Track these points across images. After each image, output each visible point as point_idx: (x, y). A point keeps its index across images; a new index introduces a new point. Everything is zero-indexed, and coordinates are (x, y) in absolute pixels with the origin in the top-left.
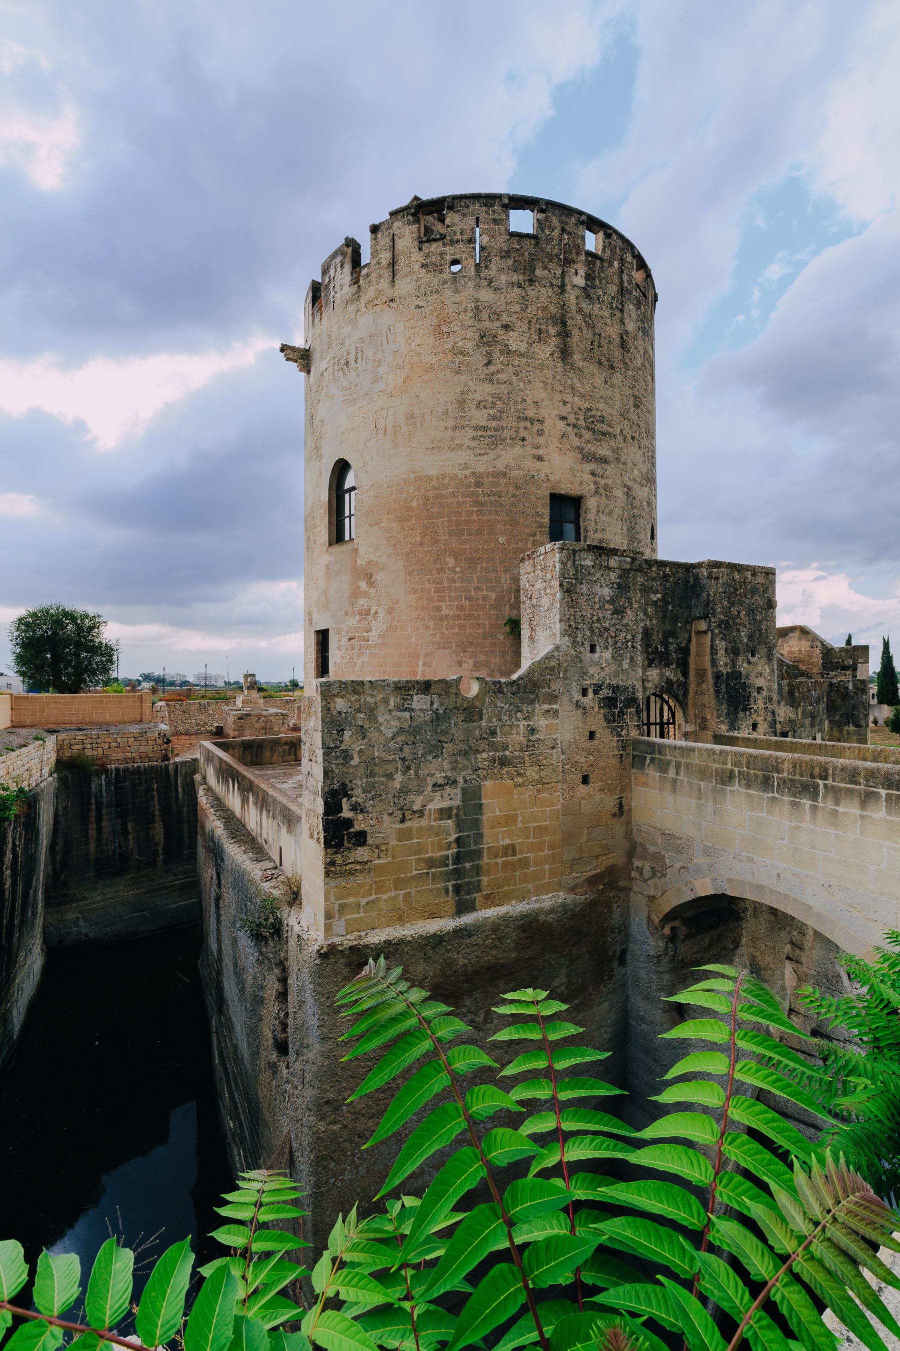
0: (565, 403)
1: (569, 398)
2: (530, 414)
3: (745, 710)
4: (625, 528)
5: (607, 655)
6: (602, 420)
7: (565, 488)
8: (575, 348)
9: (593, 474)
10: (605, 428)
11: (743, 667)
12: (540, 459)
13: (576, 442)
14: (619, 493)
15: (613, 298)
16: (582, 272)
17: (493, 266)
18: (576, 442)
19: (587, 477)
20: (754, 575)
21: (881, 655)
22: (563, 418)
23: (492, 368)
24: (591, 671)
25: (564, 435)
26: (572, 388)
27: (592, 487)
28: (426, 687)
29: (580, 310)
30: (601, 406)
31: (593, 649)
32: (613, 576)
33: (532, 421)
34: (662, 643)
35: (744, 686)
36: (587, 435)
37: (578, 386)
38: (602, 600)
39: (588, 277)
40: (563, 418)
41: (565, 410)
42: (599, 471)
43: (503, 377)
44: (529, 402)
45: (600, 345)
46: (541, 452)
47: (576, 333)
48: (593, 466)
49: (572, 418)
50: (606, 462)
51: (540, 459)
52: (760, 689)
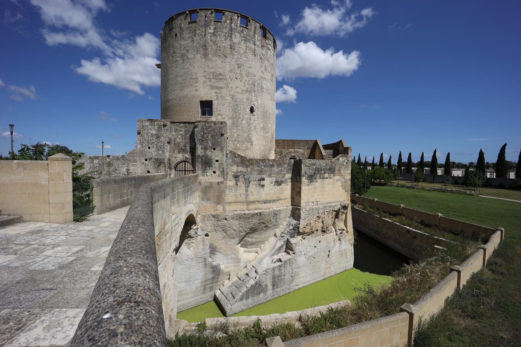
0: (205, 71)
1: (207, 70)
2: (194, 77)
3: (210, 167)
4: (231, 109)
5: (154, 149)
6: (220, 74)
7: (204, 99)
8: (209, 53)
9: (216, 93)
10: (221, 77)
11: (209, 153)
12: (197, 90)
13: (209, 83)
14: (228, 98)
15: (226, 33)
16: (212, 28)
17: (184, 33)
18: (209, 83)
19: (213, 94)
20: (215, 124)
21: (500, 150)
22: (204, 76)
23: (184, 64)
24: (148, 154)
25: (205, 82)
26: (208, 66)
27: (215, 97)
28: (97, 158)
29: (211, 40)
30: (220, 70)
31: (149, 148)
32: (156, 127)
33: (194, 79)
34: (184, 146)
35: (210, 159)
36: (214, 81)
37: (211, 65)
38: (152, 135)
39: (215, 29)
40: (204, 76)
41: (205, 74)
42: (218, 91)
43: (186, 67)
44: (194, 73)
45: (220, 50)
46: (197, 88)
47: (210, 49)
48: (215, 90)
49: (208, 76)
50: (221, 88)
51: (197, 90)
52: (217, 161)
